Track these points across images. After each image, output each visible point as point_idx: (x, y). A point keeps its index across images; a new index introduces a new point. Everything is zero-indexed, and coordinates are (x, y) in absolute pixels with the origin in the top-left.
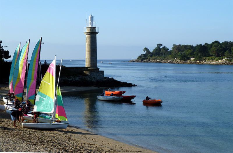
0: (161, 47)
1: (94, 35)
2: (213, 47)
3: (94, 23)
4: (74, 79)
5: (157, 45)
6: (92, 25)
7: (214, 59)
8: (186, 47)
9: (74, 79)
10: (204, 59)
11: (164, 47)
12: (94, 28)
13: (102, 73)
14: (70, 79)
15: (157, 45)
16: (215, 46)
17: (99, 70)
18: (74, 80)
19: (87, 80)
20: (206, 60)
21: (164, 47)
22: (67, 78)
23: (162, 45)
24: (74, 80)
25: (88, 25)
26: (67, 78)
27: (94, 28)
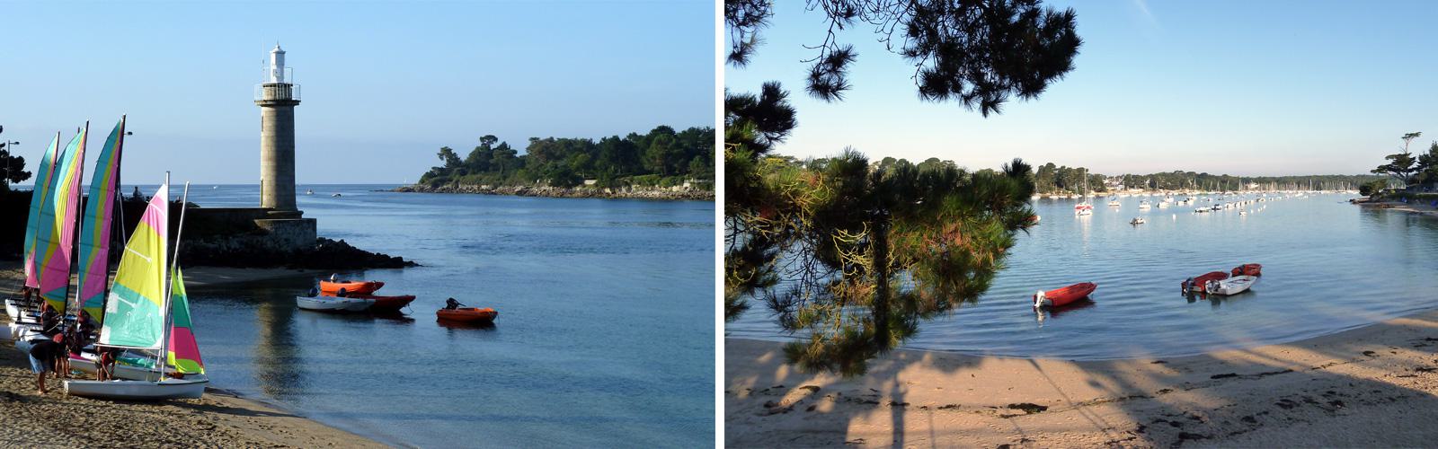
0: (494, 146)
2: (653, 144)
3: (287, 71)
4: (224, 244)
5: (482, 139)
6: (281, 76)
8: (569, 145)
10: (627, 184)
11: (504, 146)
12: (288, 87)
15: (482, 139)
16: (660, 142)
17: (303, 216)
20: (633, 186)
21: (504, 146)
23: (496, 139)
24: (225, 248)
27: (288, 87)
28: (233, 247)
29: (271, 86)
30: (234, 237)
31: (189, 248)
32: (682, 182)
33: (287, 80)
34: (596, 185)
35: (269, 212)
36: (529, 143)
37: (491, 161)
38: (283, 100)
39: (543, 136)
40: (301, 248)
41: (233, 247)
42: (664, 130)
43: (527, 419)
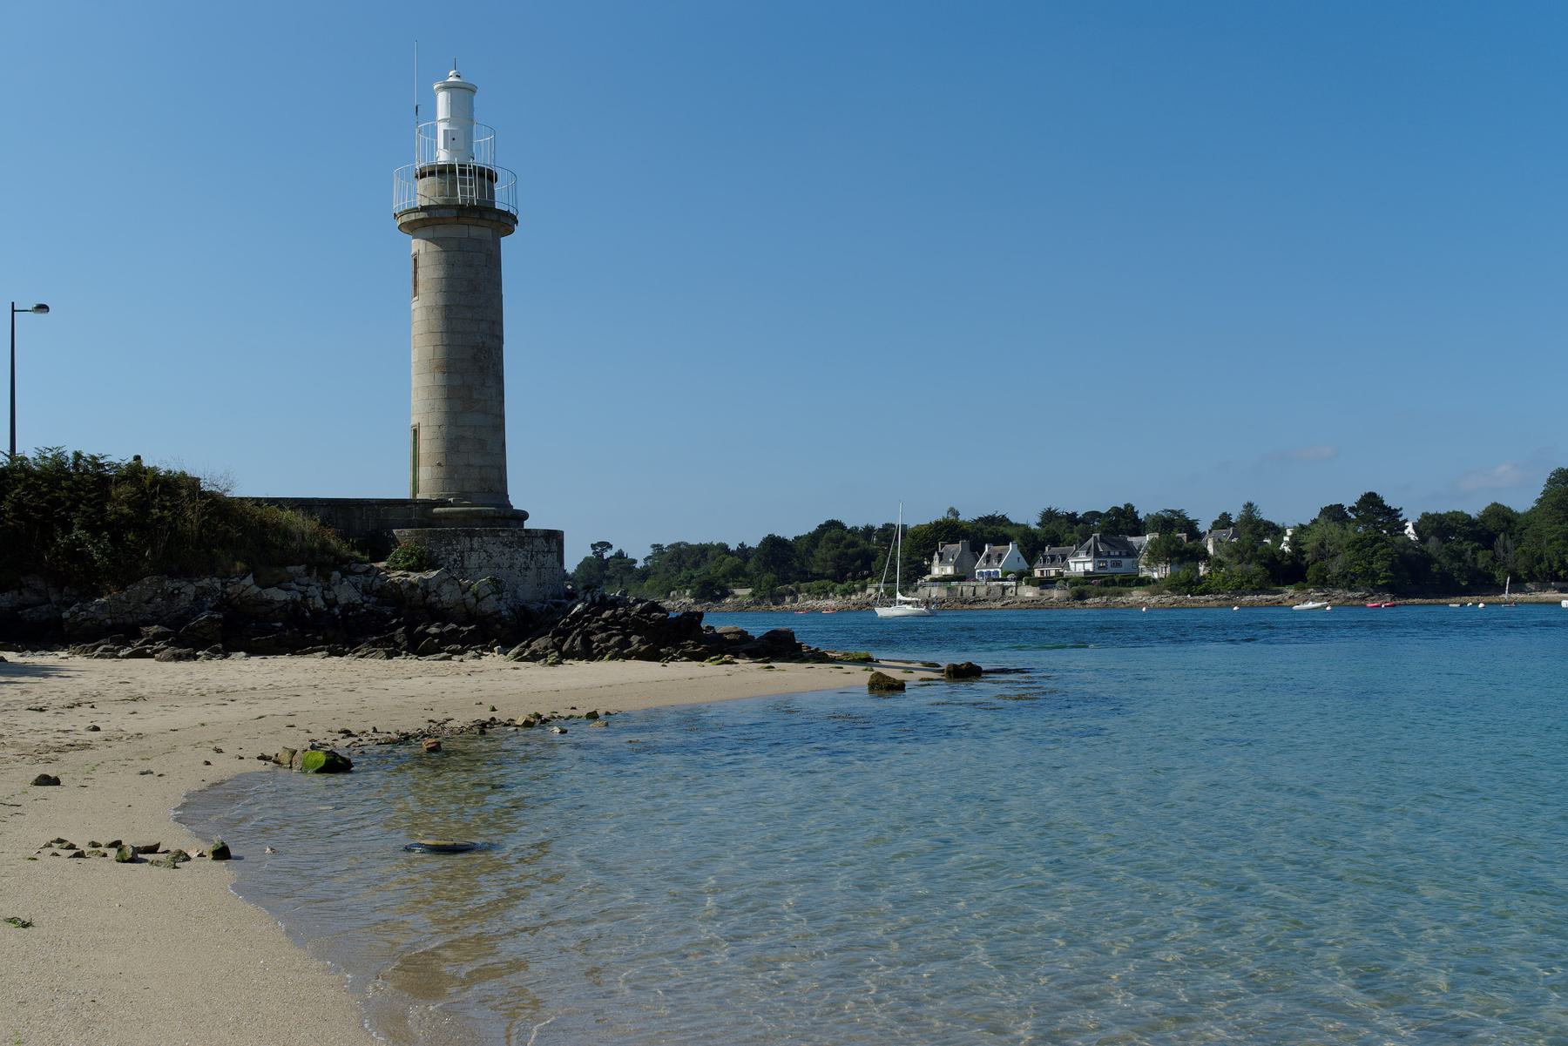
0: (607, 555)
1: (487, 233)
2: (822, 543)
3: (482, 141)
4: (315, 591)
5: (593, 546)
6: (462, 134)
7: (833, 589)
8: (703, 551)
9: (315, 591)
10: (791, 593)
11: (620, 555)
12: (487, 176)
13: (554, 547)
14: (278, 595)
15: (593, 546)
16: (831, 540)
17: (527, 525)
18: (320, 603)
19: (433, 599)
20: (800, 597)
21: (620, 555)
22: (249, 580)
23: (610, 546)
24: (320, 603)
25: (433, 147)
26: (249, 580)
27: (487, 176)
28: (342, 600)
29: (432, 174)
30: (345, 574)
31: (209, 602)
32: (864, 588)
33: (482, 160)
34: (753, 595)
35: (436, 510)
36: (650, 552)
37: (607, 573)
38: (472, 207)
39: (666, 543)
40: (535, 607)
41: (342, 600)
42: (833, 525)
43: (1083, 983)
